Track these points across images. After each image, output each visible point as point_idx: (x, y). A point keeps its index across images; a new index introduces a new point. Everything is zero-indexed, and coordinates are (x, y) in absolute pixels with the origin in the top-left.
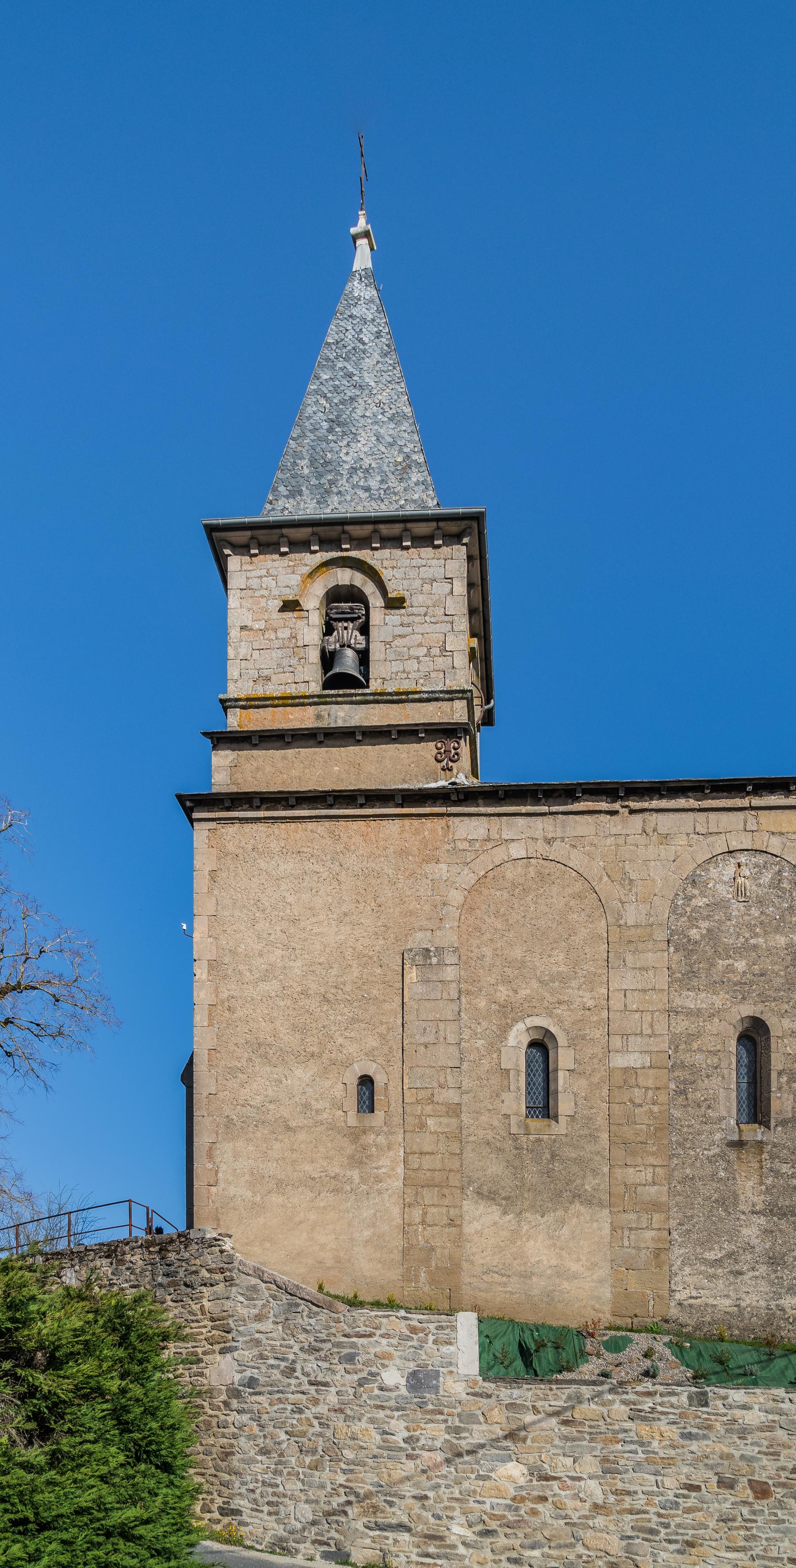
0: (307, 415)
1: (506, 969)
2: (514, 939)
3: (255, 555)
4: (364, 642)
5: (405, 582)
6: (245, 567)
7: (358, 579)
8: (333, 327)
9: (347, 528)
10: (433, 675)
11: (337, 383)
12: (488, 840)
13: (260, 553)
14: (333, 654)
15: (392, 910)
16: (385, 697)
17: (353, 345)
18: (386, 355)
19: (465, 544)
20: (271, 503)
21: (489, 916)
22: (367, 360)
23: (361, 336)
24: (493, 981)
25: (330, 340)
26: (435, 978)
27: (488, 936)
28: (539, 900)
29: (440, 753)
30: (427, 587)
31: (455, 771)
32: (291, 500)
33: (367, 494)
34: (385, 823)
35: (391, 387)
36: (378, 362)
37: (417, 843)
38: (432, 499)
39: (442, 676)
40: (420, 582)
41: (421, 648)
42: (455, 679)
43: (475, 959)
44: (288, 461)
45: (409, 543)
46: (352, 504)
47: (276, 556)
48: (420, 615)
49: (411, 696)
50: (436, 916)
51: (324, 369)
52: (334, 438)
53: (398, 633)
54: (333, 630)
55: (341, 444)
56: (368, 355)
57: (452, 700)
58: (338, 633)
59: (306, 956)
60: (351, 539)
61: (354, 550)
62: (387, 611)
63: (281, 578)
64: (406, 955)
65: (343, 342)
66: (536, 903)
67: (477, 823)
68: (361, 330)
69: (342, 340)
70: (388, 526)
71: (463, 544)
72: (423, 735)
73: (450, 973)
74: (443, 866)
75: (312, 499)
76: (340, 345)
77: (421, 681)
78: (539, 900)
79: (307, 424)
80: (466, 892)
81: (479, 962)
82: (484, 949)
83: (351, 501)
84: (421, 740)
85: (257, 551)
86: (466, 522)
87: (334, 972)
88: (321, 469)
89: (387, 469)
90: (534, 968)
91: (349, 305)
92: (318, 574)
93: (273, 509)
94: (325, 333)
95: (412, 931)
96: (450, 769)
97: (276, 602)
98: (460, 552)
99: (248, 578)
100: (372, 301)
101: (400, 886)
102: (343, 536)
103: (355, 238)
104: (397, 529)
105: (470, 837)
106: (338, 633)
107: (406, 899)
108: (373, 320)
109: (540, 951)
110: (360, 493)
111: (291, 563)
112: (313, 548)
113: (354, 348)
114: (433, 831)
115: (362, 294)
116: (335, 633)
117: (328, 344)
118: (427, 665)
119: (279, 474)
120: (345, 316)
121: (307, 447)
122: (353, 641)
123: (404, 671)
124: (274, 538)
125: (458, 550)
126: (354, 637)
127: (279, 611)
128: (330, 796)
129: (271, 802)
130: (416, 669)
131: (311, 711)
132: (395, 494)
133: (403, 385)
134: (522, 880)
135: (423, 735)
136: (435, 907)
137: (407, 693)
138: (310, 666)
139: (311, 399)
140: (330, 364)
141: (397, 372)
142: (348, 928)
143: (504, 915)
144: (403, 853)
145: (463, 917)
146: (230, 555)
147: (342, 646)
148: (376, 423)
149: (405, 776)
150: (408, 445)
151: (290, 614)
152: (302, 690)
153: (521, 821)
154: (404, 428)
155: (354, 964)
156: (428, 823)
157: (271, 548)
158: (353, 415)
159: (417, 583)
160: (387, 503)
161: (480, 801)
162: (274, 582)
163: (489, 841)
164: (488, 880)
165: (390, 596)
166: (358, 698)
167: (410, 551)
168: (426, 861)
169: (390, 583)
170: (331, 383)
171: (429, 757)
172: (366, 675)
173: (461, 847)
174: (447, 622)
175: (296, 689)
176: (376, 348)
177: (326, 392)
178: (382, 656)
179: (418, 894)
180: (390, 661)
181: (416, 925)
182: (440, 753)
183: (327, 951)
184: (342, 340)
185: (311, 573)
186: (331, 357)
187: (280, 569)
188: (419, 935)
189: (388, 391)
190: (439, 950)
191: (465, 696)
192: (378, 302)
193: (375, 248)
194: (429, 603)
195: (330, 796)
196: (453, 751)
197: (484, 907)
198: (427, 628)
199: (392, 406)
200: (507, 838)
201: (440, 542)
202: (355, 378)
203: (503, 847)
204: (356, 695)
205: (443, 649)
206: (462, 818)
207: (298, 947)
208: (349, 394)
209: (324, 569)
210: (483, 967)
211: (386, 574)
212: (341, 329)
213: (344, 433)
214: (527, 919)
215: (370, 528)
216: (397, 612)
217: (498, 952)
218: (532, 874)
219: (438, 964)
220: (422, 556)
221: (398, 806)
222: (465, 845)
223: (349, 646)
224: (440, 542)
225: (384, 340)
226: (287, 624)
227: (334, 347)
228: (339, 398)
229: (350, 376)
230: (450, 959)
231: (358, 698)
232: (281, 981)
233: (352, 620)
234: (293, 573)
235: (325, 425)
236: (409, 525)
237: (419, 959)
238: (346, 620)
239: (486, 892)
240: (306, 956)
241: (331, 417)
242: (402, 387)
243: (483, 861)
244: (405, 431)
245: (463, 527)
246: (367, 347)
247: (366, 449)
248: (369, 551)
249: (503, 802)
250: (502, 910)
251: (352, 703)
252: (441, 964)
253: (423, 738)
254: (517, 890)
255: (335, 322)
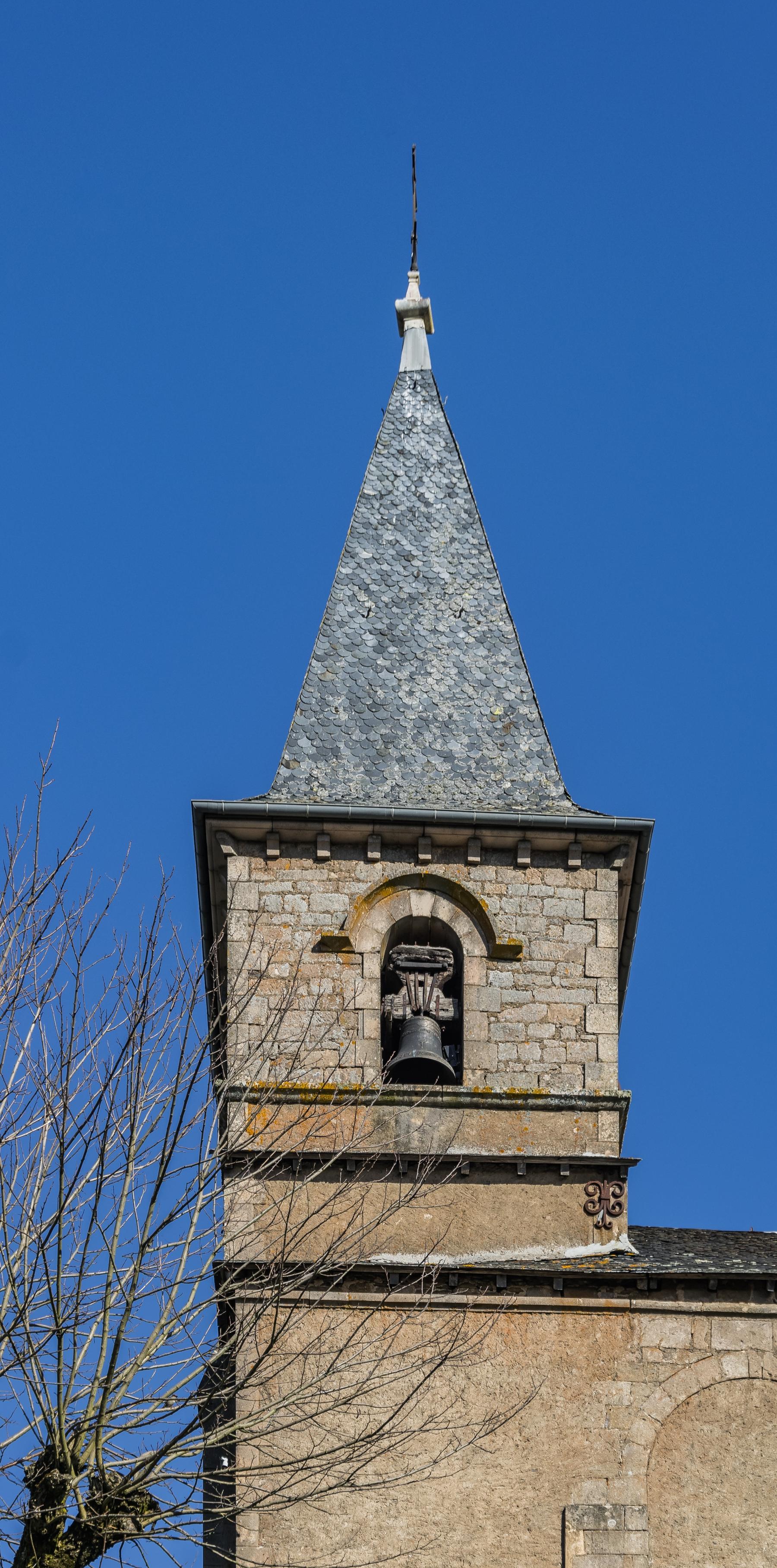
0: (338, 618)
1: (717, 1539)
2: (729, 1496)
3: (274, 858)
4: (451, 1009)
5: (520, 920)
6: (256, 876)
7: (445, 910)
8: (373, 468)
9: (430, 830)
10: (565, 1069)
11: (385, 567)
12: (692, 1349)
13: (281, 855)
14: (401, 1022)
15: (546, 1447)
16: (489, 1100)
17: (408, 504)
18: (465, 528)
19: (617, 869)
20: (287, 766)
21: (692, 1461)
22: (434, 533)
23: (422, 490)
24: (698, 1556)
25: (368, 491)
26: (612, 1550)
27: (691, 1489)
28: (766, 1441)
29: (593, 1202)
30: (555, 930)
31: (615, 1230)
32: (321, 764)
33: (447, 766)
34: (536, 1317)
35: (478, 585)
36: (453, 540)
37: (584, 1349)
38: (556, 784)
39: (579, 1070)
40: (544, 921)
41: (546, 1026)
42: (600, 1078)
43: (671, 1522)
44: (311, 695)
45: (527, 860)
46: (426, 780)
47: (309, 863)
48: (543, 973)
49: (531, 1101)
50: (612, 1457)
51: (361, 540)
52: (387, 663)
53: (510, 999)
54: (401, 985)
55: (399, 675)
56: (436, 524)
57: (596, 1110)
58: (409, 991)
59: (414, 1512)
60: (434, 846)
61: (438, 862)
62: (490, 964)
63: (316, 897)
64: (568, 1515)
65: (390, 497)
66: (761, 1444)
67: (675, 1324)
68: (420, 478)
69: (390, 492)
70: (496, 833)
71: (614, 869)
72: (567, 1173)
73: (635, 1543)
74: (625, 1386)
75: (356, 766)
76: (387, 501)
77: (547, 1077)
78: (766, 1441)
79: (339, 634)
80: (658, 1425)
81: (677, 1527)
82: (684, 1509)
83: (423, 775)
84: (562, 1180)
85: (276, 852)
86: (622, 837)
87: (457, 1536)
88: (368, 715)
89: (478, 725)
90: (758, 1539)
91: (398, 433)
92: (379, 897)
93: (292, 777)
94: (359, 479)
95: (577, 1479)
96: (608, 1227)
97: (308, 935)
98: (609, 879)
99: (261, 894)
100: (433, 429)
101: (559, 1411)
102: (422, 842)
103: (402, 316)
104: (510, 838)
105: (663, 1344)
106: (409, 991)
107: (568, 1432)
108: (441, 464)
109: (768, 1513)
110: (436, 761)
111: (333, 875)
112: (370, 855)
113: (410, 510)
114: (607, 1332)
115: (418, 415)
116: (404, 991)
117: (367, 497)
118: (555, 1052)
119: (298, 718)
120: (393, 451)
121: (341, 675)
122: (433, 1005)
123: (518, 1060)
124: (309, 835)
125: (606, 877)
126: (434, 998)
127: (314, 950)
128: (454, 1274)
129: (359, 1278)
130: (538, 1057)
131: (366, 1116)
132: (495, 769)
133: (497, 584)
134: (740, 1410)
135: (567, 1173)
136: (612, 1445)
137: (526, 1096)
138: (366, 1042)
139: (342, 592)
140: (371, 532)
141: (486, 559)
142: (479, 1471)
143: (715, 1459)
144: (564, 1363)
145: (653, 1461)
146: (231, 855)
147: (416, 1013)
148: (455, 644)
149: (537, 1233)
150: (512, 687)
151: (332, 957)
152: (352, 1079)
153: (740, 1324)
154: (502, 659)
155: (489, 1525)
156: (601, 1322)
157: (299, 849)
158: (417, 627)
159: (540, 923)
160: (482, 784)
161: (680, 1292)
162: (305, 903)
163: (692, 1351)
164: (691, 1407)
165: (498, 942)
166: (446, 1099)
167: (528, 871)
168: (600, 1375)
169: (497, 919)
170: (375, 566)
171: (576, 1206)
172: (457, 1059)
173: (651, 1359)
174: (587, 988)
175: (342, 1077)
176: (447, 515)
177: (368, 581)
178: (484, 1035)
179: (586, 1424)
180: (496, 1043)
181: (583, 1471)
182: (593, 1202)
183: (447, 1503)
184: (390, 492)
185: (369, 896)
186: (374, 521)
187: (315, 883)
188: (588, 1485)
189: (472, 591)
190: (619, 1509)
191: (617, 1105)
192: (447, 433)
193: (433, 331)
194: (560, 955)
195: (454, 1274)
196: (613, 1201)
197: (684, 1447)
198: (555, 995)
199: (481, 619)
200: (719, 1347)
201: (578, 862)
202: (416, 563)
203: (714, 1361)
204: (442, 1094)
205: (582, 1029)
206: (652, 1316)
207: (400, 1497)
208: (407, 589)
209: (390, 890)
210: (683, 1535)
211: (491, 905)
212: (386, 473)
213: (404, 658)
214: (749, 1467)
215: (468, 832)
216: (508, 966)
217: (706, 1514)
218: (757, 1402)
219: (617, 1529)
220: (548, 880)
221: (555, 1293)
222: (657, 1356)
223: (427, 1014)
224: (578, 862)
225: (460, 501)
226: (327, 972)
227: (377, 505)
228: (390, 594)
229: (408, 558)
230: (635, 1522)
231: (446, 1099)
232: (374, 1547)
233: (432, 972)
234: (337, 891)
235: (371, 640)
236: (530, 835)
237: (589, 1521)
238: (422, 971)
239: (687, 1425)
240: (414, 1512)
241: (379, 626)
242: (494, 588)
243: (683, 1380)
244: (504, 663)
245: (616, 844)
246: (433, 511)
247: (443, 689)
248: (462, 866)
249: (714, 1295)
250: (712, 1453)
251: (434, 1105)
252: (622, 1529)
253: (565, 1177)
254: (734, 1425)
255: (375, 459)
